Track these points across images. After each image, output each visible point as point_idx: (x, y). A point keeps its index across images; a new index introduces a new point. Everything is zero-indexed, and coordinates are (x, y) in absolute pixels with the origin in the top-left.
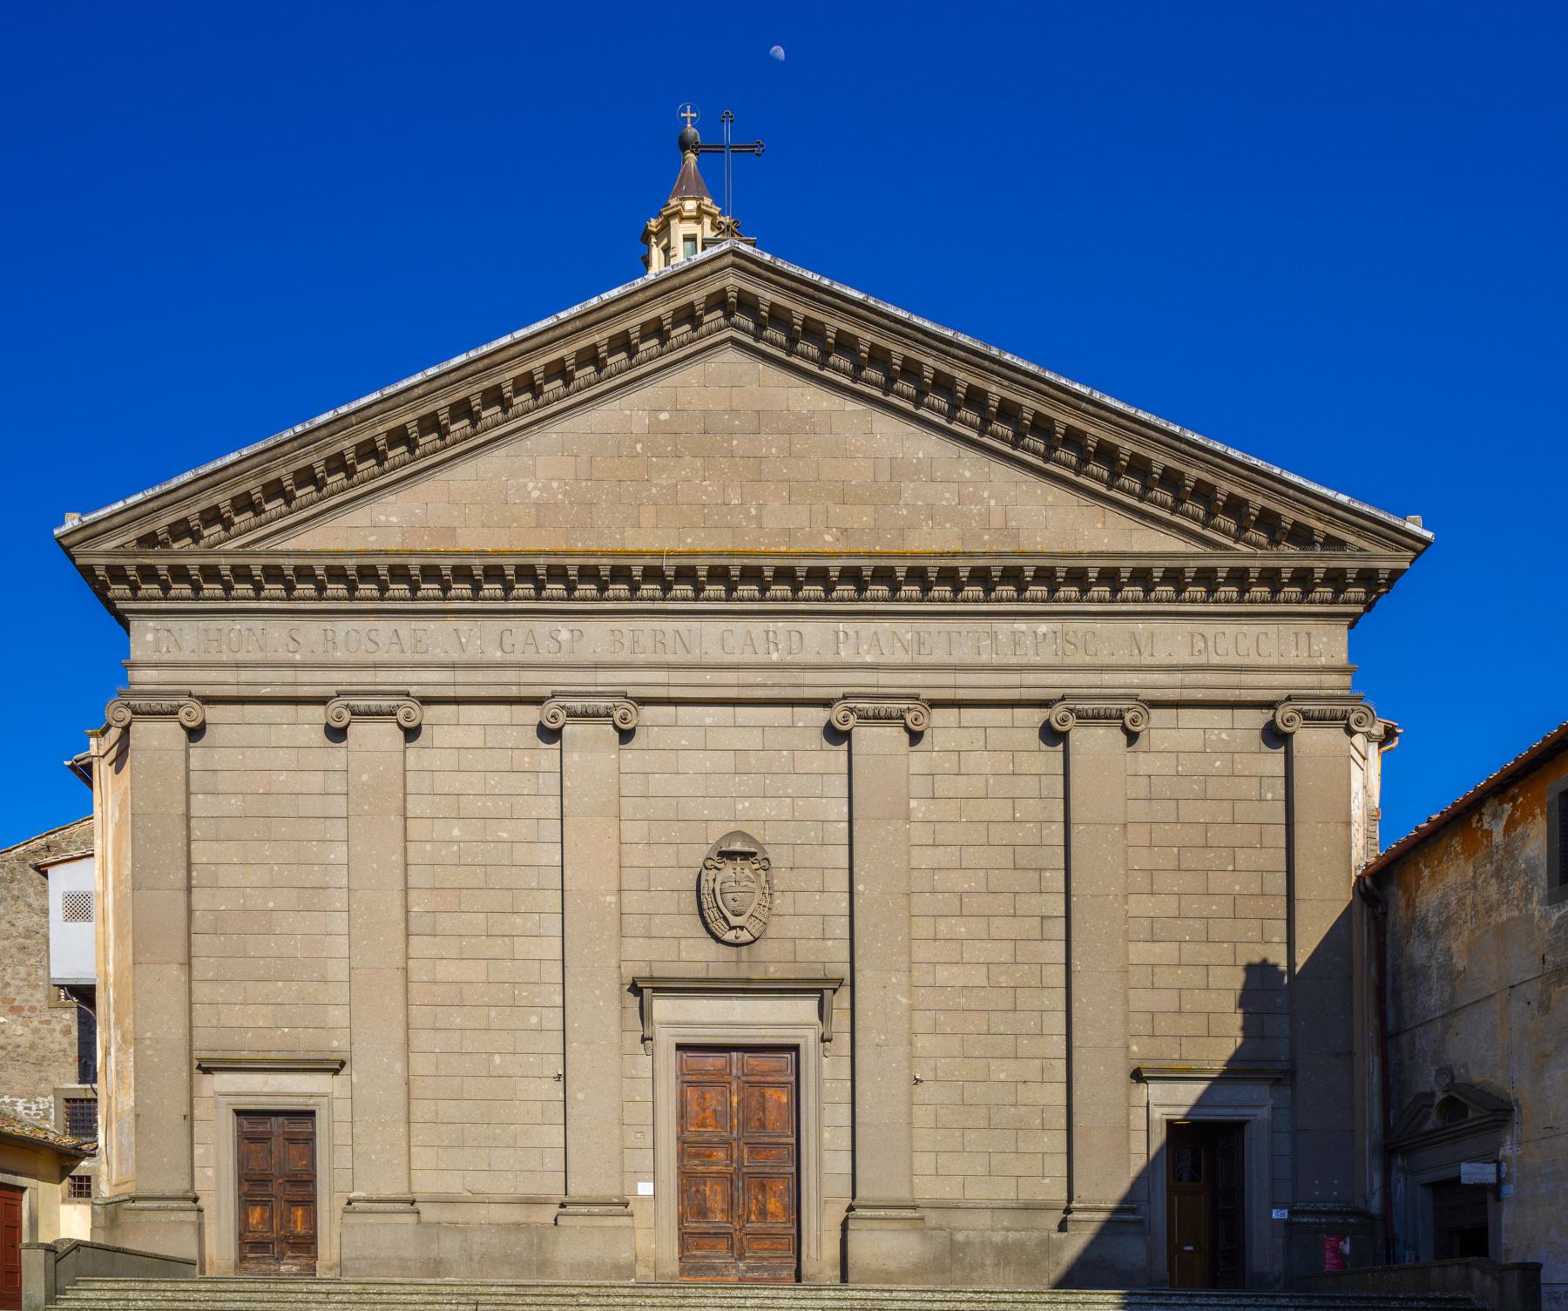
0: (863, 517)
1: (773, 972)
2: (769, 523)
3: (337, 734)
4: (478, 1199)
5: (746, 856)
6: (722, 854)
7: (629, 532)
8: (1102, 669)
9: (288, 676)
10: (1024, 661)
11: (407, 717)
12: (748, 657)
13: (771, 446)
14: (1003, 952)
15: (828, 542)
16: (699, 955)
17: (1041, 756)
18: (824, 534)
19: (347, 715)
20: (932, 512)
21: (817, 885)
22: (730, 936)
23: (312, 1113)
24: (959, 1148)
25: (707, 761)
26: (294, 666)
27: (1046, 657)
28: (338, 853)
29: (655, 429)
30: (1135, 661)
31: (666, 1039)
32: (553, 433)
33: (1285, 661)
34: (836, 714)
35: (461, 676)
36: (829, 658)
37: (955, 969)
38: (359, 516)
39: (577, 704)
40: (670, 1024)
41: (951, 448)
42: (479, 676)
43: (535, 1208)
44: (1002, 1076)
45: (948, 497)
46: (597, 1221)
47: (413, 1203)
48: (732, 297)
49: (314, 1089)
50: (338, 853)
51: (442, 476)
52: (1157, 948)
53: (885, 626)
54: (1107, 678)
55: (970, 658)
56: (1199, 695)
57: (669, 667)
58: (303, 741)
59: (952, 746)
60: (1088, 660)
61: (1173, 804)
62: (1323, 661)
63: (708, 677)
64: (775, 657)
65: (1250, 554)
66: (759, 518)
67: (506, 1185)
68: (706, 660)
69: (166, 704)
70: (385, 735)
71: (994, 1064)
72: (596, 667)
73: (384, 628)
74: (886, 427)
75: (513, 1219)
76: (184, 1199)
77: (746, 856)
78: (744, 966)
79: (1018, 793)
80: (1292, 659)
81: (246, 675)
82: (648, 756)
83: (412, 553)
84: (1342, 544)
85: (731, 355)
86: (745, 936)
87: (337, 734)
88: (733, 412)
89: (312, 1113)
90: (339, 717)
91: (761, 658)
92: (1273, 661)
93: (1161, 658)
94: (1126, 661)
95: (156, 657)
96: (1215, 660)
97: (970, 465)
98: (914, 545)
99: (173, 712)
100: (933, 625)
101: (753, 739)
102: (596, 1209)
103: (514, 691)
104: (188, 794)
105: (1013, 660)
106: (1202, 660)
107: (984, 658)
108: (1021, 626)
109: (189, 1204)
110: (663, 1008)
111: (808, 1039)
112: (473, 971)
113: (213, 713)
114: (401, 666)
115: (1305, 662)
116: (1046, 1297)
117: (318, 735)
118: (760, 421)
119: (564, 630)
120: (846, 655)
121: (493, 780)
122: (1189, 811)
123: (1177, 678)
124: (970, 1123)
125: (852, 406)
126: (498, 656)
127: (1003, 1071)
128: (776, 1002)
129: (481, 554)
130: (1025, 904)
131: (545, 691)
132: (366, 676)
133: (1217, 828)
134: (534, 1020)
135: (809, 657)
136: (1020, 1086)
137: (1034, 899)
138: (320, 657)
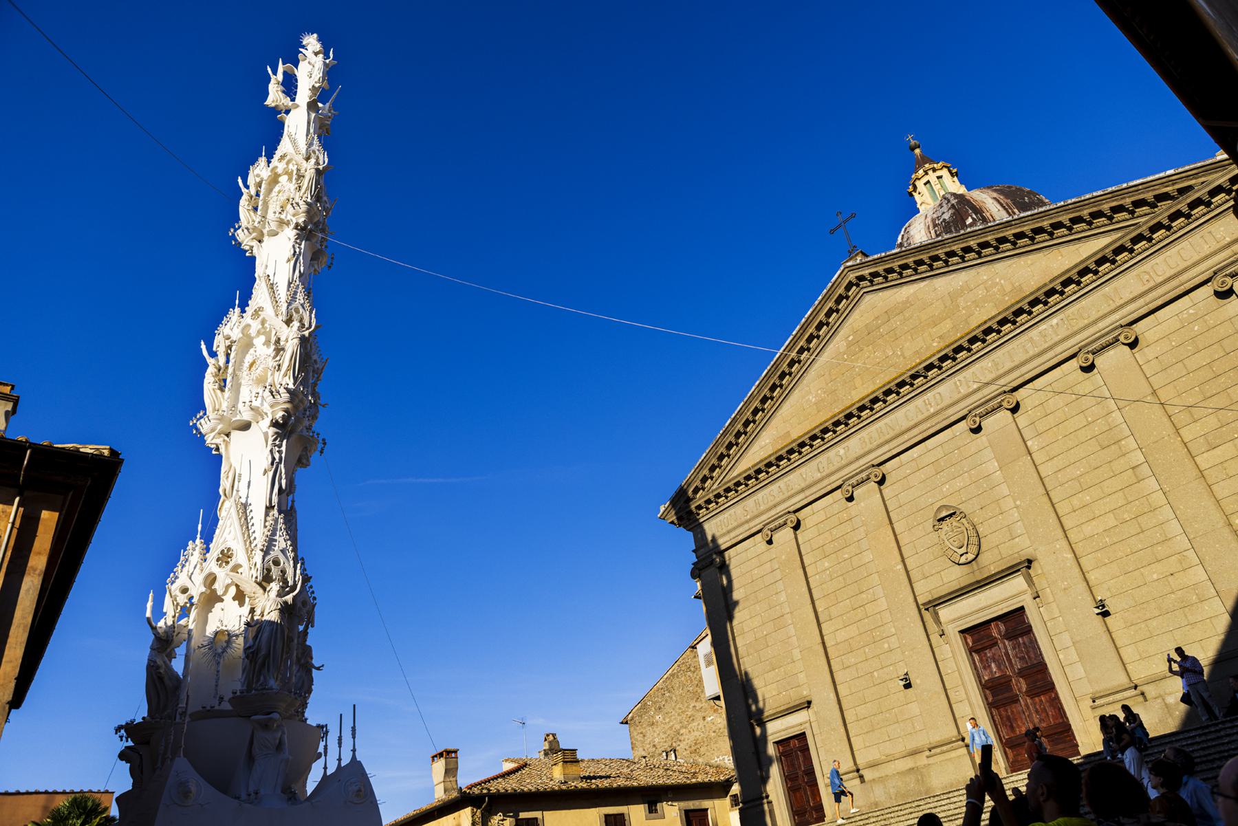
0: (947, 325)
1: (993, 570)
2: (907, 354)
3: (1089, 369)
4: (890, 759)
5: (951, 515)
6: (939, 520)
7: (853, 393)
8: (1095, 322)
9: (746, 527)
10: (1042, 348)
11: (1126, 338)
12: (921, 417)
13: (896, 321)
14: (1118, 499)
15: (936, 345)
16: (955, 577)
17: (1087, 382)
18: (931, 344)
19: (1090, 356)
20: (976, 303)
21: (997, 511)
22: (963, 560)
23: (1022, 608)
24: (1148, 635)
25: (921, 475)
26: (747, 522)
27: (1063, 333)
28: (783, 598)
29: (849, 346)
30: (1113, 306)
31: (953, 631)
32: (812, 372)
33: (1203, 255)
34: (1215, 285)
35: (808, 492)
36: (956, 397)
37: (1094, 523)
38: (755, 447)
39: (854, 481)
40: (954, 620)
41: (973, 272)
42: (814, 489)
43: (917, 756)
44: (1155, 576)
45: (981, 292)
46: (947, 756)
47: (1136, 687)
48: (854, 281)
49: (801, 721)
50: (783, 598)
51: (778, 414)
52: (1218, 451)
53: (977, 366)
54: (1101, 325)
55: (1024, 357)
56: (1160, 302)
57: (887, 442)
58: (759, 551)
59: (1037, 403)
60: (1086, 322)
61: (1180, 364)
62: (1228, 239)
63: (906, 437)
64: (932, 410)
65: (1144, 219)
66: (902, 355)
67: (901, 747)
68: (903, 429)
69: (1110, 338)
70: (1120, 353)
71: (1145, 571)
72: (857, 459)
73: (774, 488)
74: (940, 283)
75: (908, 767)
76: (1130, 688)
77: (951, 515)
78: (977, 573)
79: (1084, 408)
80: (1207, 250)
81: (733, 534)
82: (895, 487)
83: (863, 399)
84: (1190, 188)
85: (868, 298)
86: (971, 556)
87: (770, 542)
88: (877, 318)
89: (1022, 608)
90: (1087, 359)
91: (926, 414)
92: (1196, 258)
93: (1127, 296)
94: (1109, 309)
95: (1028, 356)
96: (1160, 279)
97: (984, 273)
98: (794, 436)
99: (785, 524)
100: (999, 353)
101: (939, 453)
102: (944, 748)
103: (829, 488)
104: (1025, 442)
105: (1046, 345)
106: (1152, 284)
107: (1031, 353)
108: (1043, 327)
109: (1133, 692)
110: (945, 613)
111: (1027, 601)
112: (853, 631)
113: (801, 515)
114: (784, 501)
115: (1218, 246)
116: (938, 810)
117: (764, 545)
118: (888, 314)
119: (840, 450)
120: (964, 391)
121: (834, 531)
122: (1192, 363)
123: (1141, 301)
124: (1148, 616)
125: (922, 284)
126: (819, 475)
127: (1153, 573)
128: (1002, 586)
129: (761, 461)
130: (1120, 465)
131: (1075, 349)
132: (773, 512)
133: (1218, 362)
134: (886, 646)
135: (948, 402)
136: (1170, 578)
137: (1122, 461)
138: (756, 513)
